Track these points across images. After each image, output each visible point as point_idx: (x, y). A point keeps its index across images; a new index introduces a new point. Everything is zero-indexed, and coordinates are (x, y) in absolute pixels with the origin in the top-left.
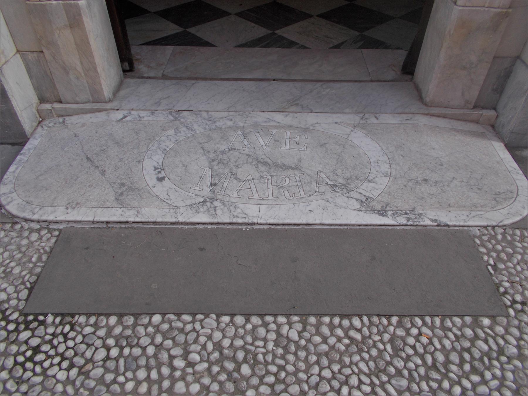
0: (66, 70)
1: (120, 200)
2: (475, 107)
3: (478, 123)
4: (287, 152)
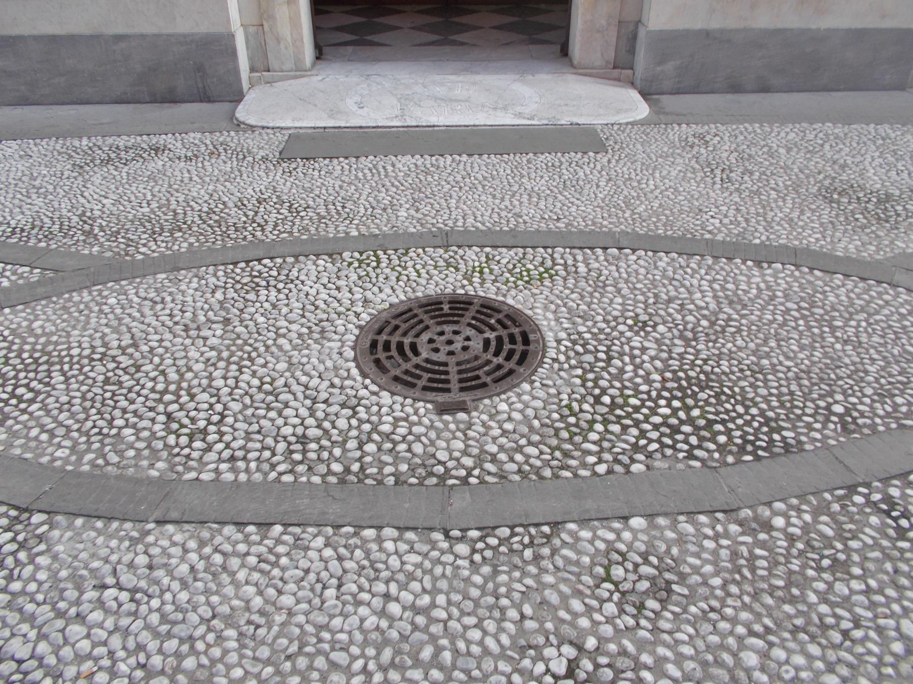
0: (278, 40)
1: (331, 117)
2: (614, 68)
3: (619, 80)
4: (458, 92)
